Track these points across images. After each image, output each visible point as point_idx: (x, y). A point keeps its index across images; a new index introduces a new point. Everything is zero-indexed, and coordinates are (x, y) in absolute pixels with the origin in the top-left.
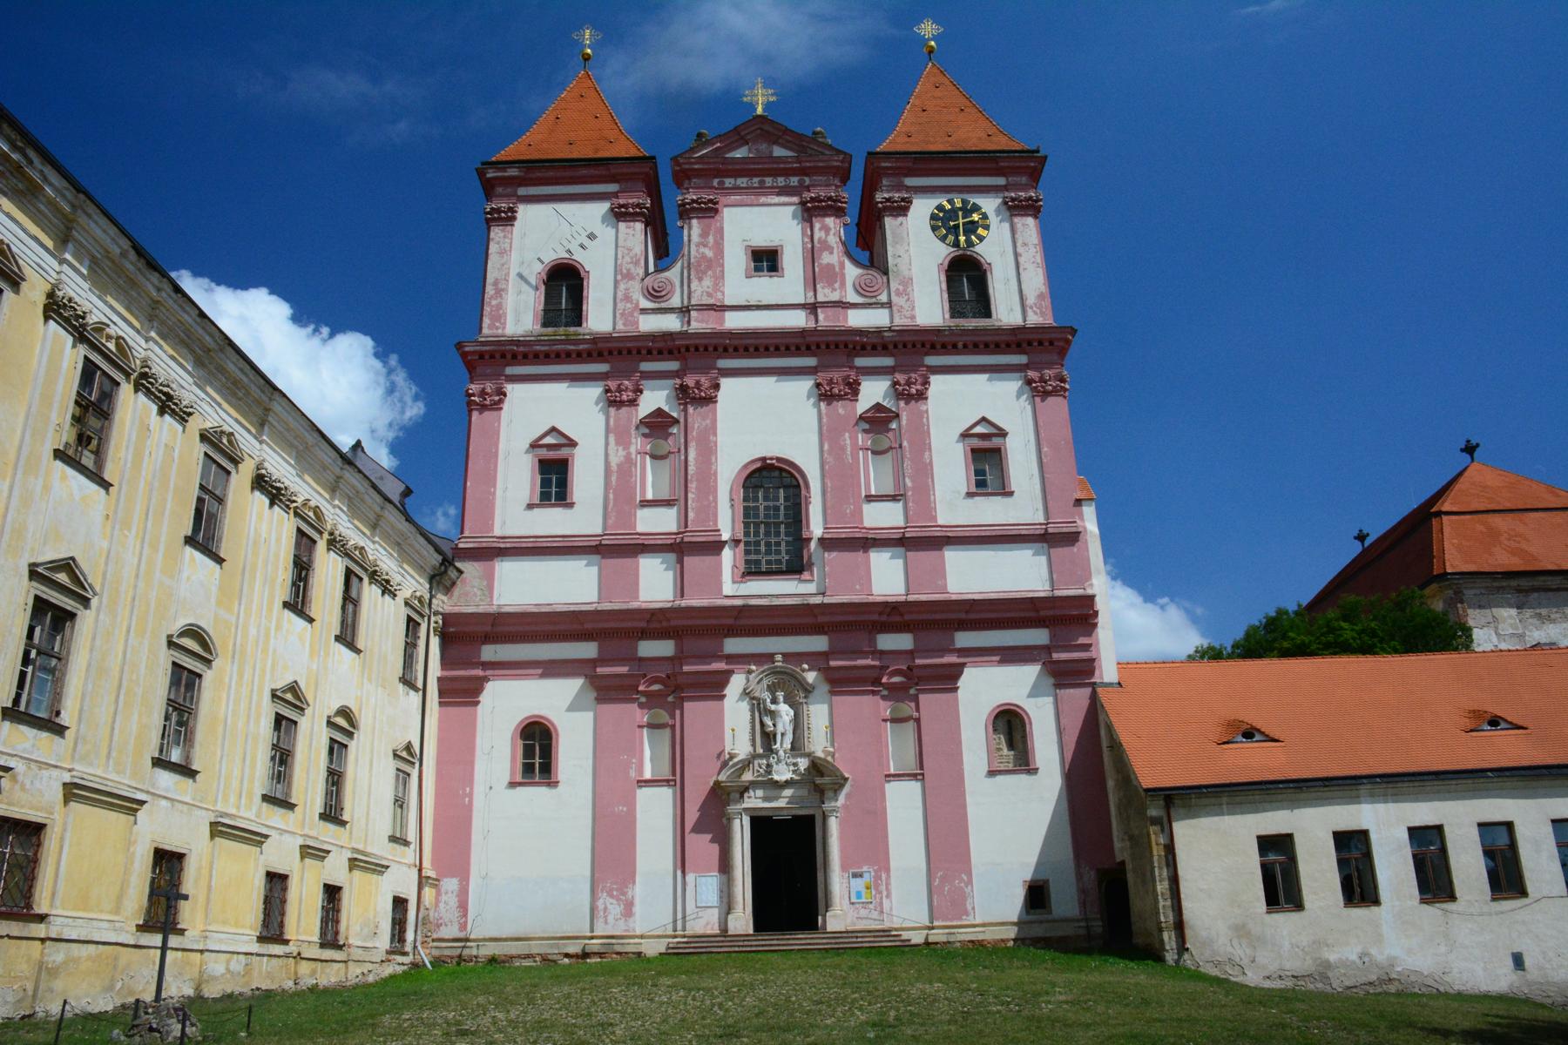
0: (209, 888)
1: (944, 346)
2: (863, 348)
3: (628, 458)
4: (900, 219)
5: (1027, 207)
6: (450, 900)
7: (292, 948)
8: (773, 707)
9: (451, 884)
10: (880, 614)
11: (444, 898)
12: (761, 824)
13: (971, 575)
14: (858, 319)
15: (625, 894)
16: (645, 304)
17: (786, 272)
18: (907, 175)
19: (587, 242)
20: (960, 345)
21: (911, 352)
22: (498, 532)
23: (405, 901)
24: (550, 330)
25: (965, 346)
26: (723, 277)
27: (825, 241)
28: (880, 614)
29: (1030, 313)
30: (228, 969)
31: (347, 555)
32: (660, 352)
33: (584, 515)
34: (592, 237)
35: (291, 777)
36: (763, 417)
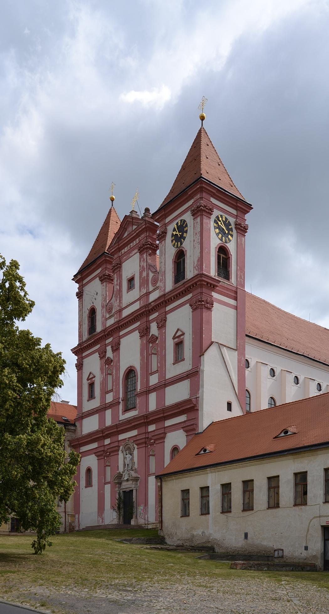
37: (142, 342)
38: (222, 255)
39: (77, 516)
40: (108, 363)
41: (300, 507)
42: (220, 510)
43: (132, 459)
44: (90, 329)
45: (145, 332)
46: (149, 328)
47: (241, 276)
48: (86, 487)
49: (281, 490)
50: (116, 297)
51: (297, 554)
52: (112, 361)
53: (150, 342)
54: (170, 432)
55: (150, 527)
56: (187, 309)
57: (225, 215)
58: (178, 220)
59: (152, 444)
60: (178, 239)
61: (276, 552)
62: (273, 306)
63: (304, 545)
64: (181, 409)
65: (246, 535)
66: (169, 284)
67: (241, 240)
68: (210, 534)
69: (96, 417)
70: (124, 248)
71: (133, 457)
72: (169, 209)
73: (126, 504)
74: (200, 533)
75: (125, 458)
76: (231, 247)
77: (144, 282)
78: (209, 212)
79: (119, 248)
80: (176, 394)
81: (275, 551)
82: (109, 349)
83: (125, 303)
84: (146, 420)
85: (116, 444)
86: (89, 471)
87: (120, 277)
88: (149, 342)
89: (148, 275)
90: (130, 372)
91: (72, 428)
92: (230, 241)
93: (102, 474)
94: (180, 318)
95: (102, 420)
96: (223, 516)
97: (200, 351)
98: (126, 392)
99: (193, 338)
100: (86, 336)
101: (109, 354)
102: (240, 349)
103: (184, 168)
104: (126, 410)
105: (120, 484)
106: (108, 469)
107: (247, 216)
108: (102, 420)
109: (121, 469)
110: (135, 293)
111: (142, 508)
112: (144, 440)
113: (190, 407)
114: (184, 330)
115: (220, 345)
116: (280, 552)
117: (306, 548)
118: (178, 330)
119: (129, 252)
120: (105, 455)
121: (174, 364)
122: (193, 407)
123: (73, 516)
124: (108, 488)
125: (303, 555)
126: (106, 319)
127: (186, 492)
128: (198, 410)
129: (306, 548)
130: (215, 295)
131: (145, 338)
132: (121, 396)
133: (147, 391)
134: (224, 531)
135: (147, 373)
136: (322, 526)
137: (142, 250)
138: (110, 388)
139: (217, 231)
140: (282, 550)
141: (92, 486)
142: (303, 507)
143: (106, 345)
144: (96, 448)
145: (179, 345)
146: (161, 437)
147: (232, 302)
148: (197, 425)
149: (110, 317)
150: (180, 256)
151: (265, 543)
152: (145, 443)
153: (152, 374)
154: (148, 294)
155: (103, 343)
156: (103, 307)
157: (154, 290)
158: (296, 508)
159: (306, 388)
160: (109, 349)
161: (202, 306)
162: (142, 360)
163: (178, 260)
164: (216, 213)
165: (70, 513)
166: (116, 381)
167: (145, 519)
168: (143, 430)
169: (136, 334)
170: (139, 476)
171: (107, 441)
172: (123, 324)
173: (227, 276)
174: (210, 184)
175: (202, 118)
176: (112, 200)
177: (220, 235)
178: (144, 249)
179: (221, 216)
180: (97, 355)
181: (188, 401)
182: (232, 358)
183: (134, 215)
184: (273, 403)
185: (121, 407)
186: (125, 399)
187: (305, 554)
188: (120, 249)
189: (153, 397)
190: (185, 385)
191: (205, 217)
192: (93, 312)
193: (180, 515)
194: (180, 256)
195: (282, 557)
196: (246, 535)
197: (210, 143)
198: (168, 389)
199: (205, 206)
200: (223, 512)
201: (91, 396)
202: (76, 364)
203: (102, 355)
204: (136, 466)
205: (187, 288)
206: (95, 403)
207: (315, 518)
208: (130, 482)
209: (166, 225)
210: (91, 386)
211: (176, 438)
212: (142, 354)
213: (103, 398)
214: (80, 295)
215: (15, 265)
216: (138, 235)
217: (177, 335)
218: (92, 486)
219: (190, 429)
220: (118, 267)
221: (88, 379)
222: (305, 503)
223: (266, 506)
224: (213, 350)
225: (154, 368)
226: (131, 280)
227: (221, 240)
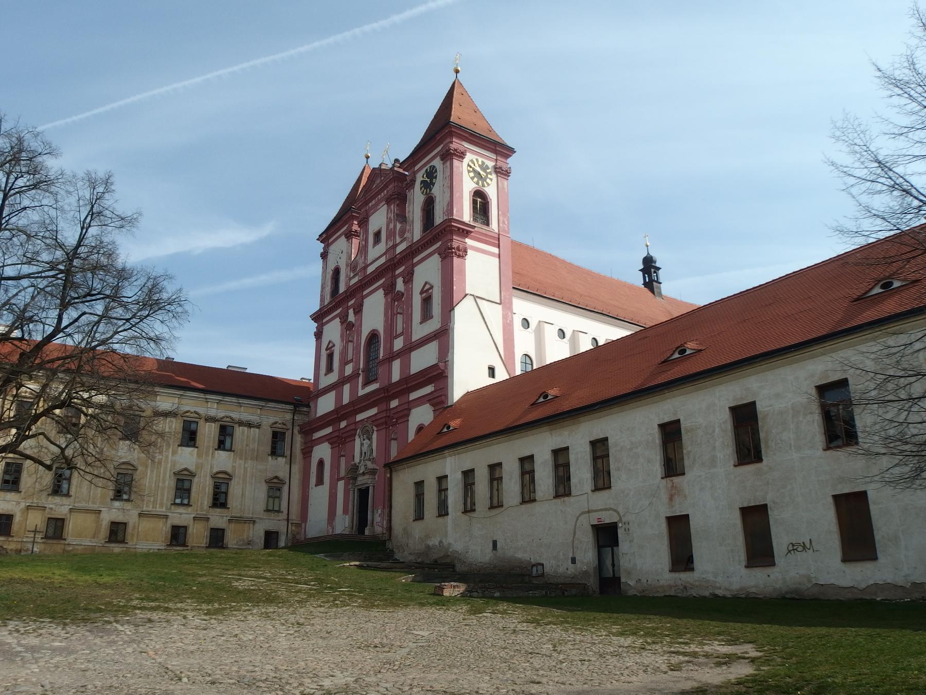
37: (386, 300)
38: (479, 200)
39: (303, 525)
40: (349, 328)
41: (562, 499)
42: (461, 508)
43: (370, 445)
45: (389, 289)
46: (395, 284)
47: (504, 222)
49: (537, 475)
50: (361, 253)
51: (561, 570)
52: (353, 325)
53: (396, 301)
56: (436, 258)
57: (480, 160)
58: (428, 167)
59: (394, 425)
60: (427, 185)
61: (534, 569)
62: (571, 265)
63: (571, 555)
65: (495, 543)
66: (417, 232)
67: (503, 184)
68: (450, 544)
69: (332, 394)
71: (372, 443)
74: (437, 544)
75: (362, 444)
76: (491, 191)
77: (391, 234)
78: (462, 156)
81: (533, 566)
82: (351, 311)
83: (371, 257)
84: (388, 392)
85: (353, 427)
86: (321, 463)
87: (367, 232)
88: (393, 300)
89: (395, 226)
90: (374, 336)
91: (305, 409)
92: (488, 185)
93: (335, 465)
94: (427, 271)
95: (339, 398)
96: (465, 518)
97: (449, 307)
98: (368, 361)
100: (327, 300)
101: (351, 317)
102: (505, 303)
103: (436, 117)
104: (367, 383)
105: (355, 479)
106: (343, 460)
107: (509, 160)
108: (339, 398)
109: (357, 460)
110: (382, 247)
111: (379, 511)
112: (383, 420)
113: (439, 375)
114: (431, 282)
115: (476, 298)
116: (540, 567)
117: (574, 561)
118: (426, 283)
119: (377, 204)
120: (340, 441)
123: (298, 525)
124: (341, 484)
125: (569, 572)
126: (350, 279)
127: (419, 485)
128: (447, 377)
129: (574, 561)
130: (469, 241)
131: (389, 296)
132: (361, 366)
133: (391, 358)
134: (467, 539)
135: (391, 335)
136: (593, 526)
137: (388, 201)
138: (350, 357)
139: (472, 174)
140: (542, 565)
142: (566, 499)
143: (348, 308)
145: (427, 301)
146: (404, 414)
147: (496, 250)
148: (446, 396)
149: (354, 277)
150: (429, 203)
151: (520, 555)
152: (386, 423)
153: (397, 336)
154: (395, 246)
155: (345, 306)
156: (347, 265)
157: (401, 242)
158: (558, 501)
159: (574, 342)
160: (351, 311)
161: (449, 255)
162: (386, 321)
164: (469, 157)
166: (357, 349)
169: (381, 292)
171: (343, 424)
172: (366, 282)
173: (487, 223)
174: (460, 127)
175: (457, 72)
176: (367, 157)
177: (476, 179)
179: (477, 160)
180: (338, 320)
181: (435, 366)
182: (494, 314)
183: (383, 167)
184: (528, 361)
185: (361, 379)
186: (367, 370)
187: (572, 569)
189: (396, 365)
190: (433, 347)
191: (455, 161)
192: (337, 271)
193: (412, 518)
194: (429, 203)
195: (543, 575)
196: (495, 543)
197: (464, 93)
198: (414, 355)
199: (456, 150)
200: (465, 512)
201: (330, 369)
203: (344, 319)
204: (374, 454)
205: (435, 235)
206: (333, 378)
207: (583, 513)
208: (367, 477)
209: (415, 173)
210: (330, 357)
211: (422, 415)
212: (386, 314)
213: (342, 370)
214: (324, 256)
215: (88, 174)
216: (386, 186)
219: (439, 400)
220: (364, 223)
221: (327, 350)
222: (568, 494)
223: (519, 499)
224: (468, 303)
225: (399, 330)
226: (377, 235)
227: (477, 183)
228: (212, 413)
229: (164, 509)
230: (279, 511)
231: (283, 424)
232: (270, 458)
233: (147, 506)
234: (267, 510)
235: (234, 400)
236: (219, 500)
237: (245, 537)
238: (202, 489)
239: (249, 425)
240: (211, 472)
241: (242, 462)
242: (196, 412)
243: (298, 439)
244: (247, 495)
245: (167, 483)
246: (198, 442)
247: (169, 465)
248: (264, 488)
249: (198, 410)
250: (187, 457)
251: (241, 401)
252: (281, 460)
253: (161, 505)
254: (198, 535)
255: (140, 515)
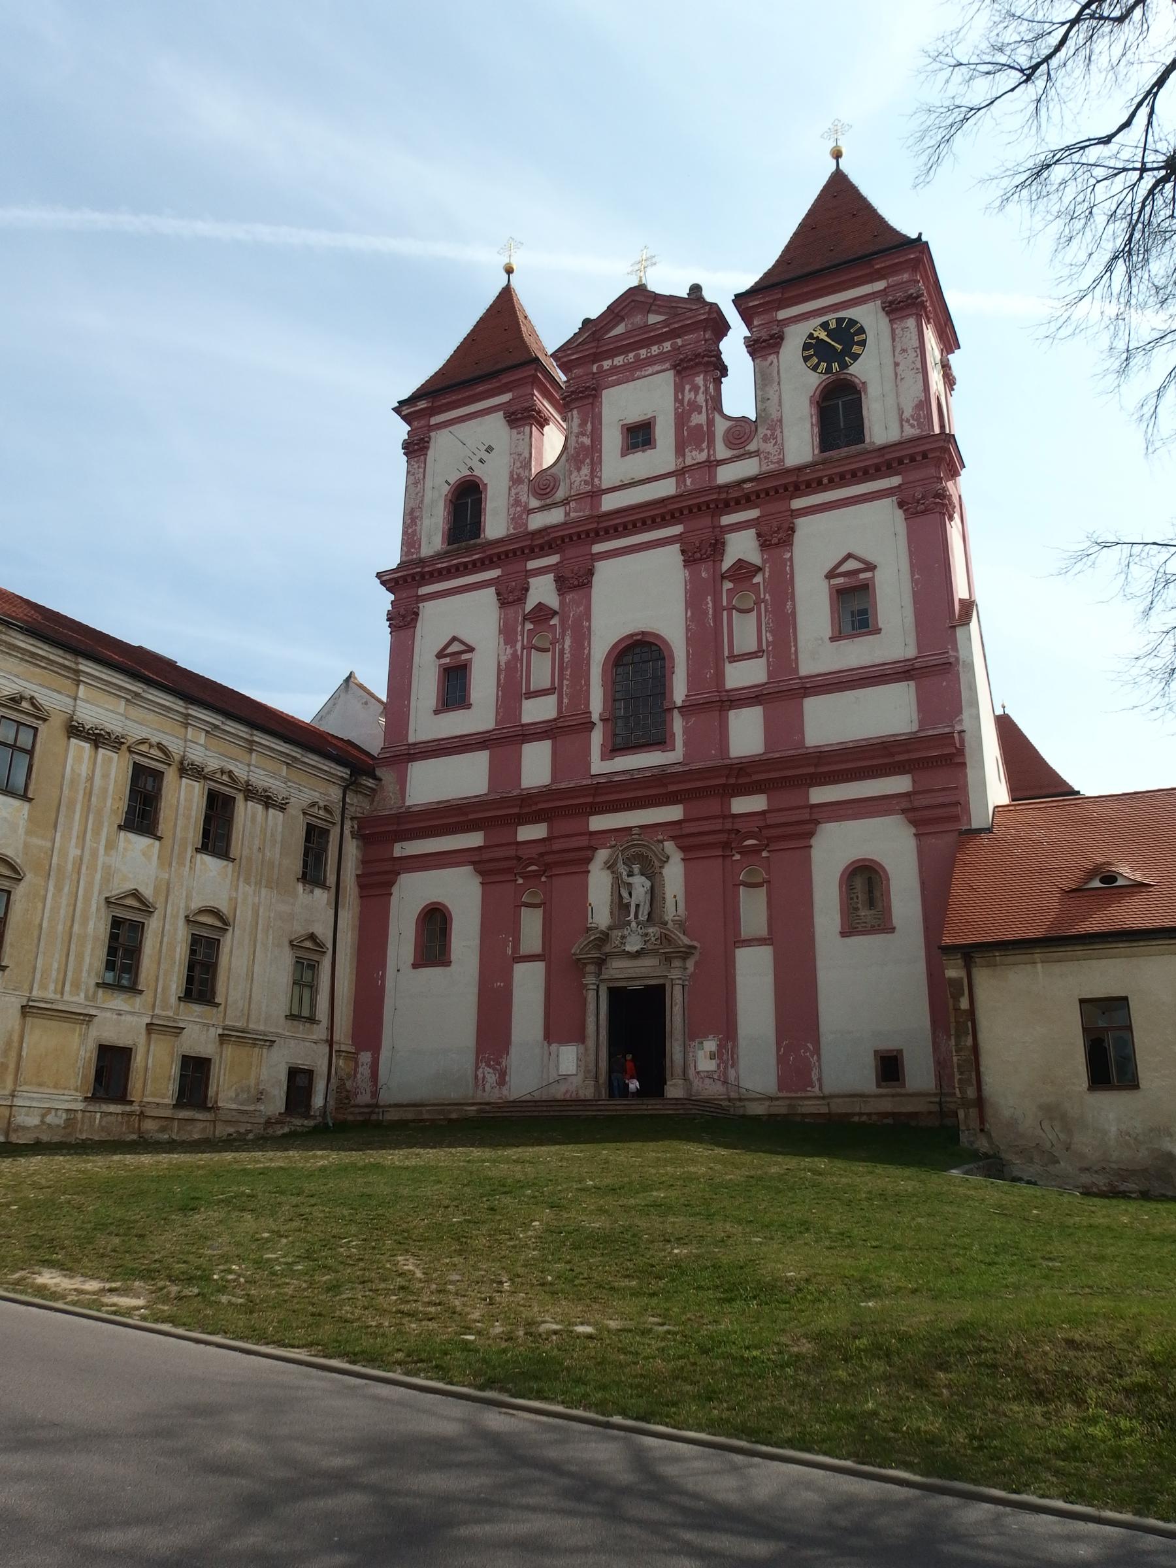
0: (20, 1056)
1: (808, 485)
2: (727, 505)
3: (514, 654)
4: (772, 358)
5: (908, 306)
6: (364, 1071)
7: (136, 1108)
8: (630, 880)
9: (365, 1057)
10: (727, 777)
11: (360, 1069)
12: (616, 994)
13: (829, 722)
14: (726, 475)
15: (499, 1064)
16: (534, 503)
17: (658, 443)
18: (779, 308)
19: (485, 456)
20: (825, 481)
21: (777, 496)
22: (411, 740)
23: (310, 1073)
24: (455, 546)
25: (831, 480)
26: (600, 462)
27: (695, 402)
28: (727, 777)
29: (906, 427)
30: (43, 1122)
31: (205, 778)
32: (542, 548)
33: (480, 715)
34: (489, 449)
35: (138, 968)
36: (641, 591)
39: (365, 1057)
44: (450, 529)
48: (415, 966)
54: (831, 819)
55: (757, 1109)
64: (534, 808)
69: (481, 759)
70: (612, 357)
72: (829, 282)
73: (637, 1028)
79: (595, 354)
80: (889, 712)
91: (370, 783)
99: (914, 582)
100: (433, 542)
112: (723, 837)
118: (454, 639)
121: (437, 712)
122: (951, 756)
128: (964, 765)
141: (447, 963)
144: (480, 848)
152: (726, 845)
153: (532, 695)
163: (457, 499)
165: (343, 1048)
167: (725, 1082)
168: (711, 806)
170: (695, 943)
175: (509, 271)
178: (697, 364)
185: (597, 738)
188: (597, 357)
202: (389, 613)
217: (449, 650)
218: (447, 963)
228: (197, 755)
229: (81, 998)
230: (312, 1020)
231: (326, 809)
232: (300, 887)
233: (43, 987)
234: (291, 1017)
235: (242, 730)
236: (200, 983)
237: (253, 1082)
238: (165, 952)
239: (268, 801)
240: (187, 907)
241: (250, 890)
242: (160, 747)
243: (352, 849)
244: (256, 975)
245: (91, 925)
246: (163, 827)
247: (98, 876)
248: (287, 958)
249: (167, 741)
250: (136, 862)
251: (260, 737)
252: (321, 897)
253: (76, 985)
254: (155, 1077)
255: (26, 1010)
